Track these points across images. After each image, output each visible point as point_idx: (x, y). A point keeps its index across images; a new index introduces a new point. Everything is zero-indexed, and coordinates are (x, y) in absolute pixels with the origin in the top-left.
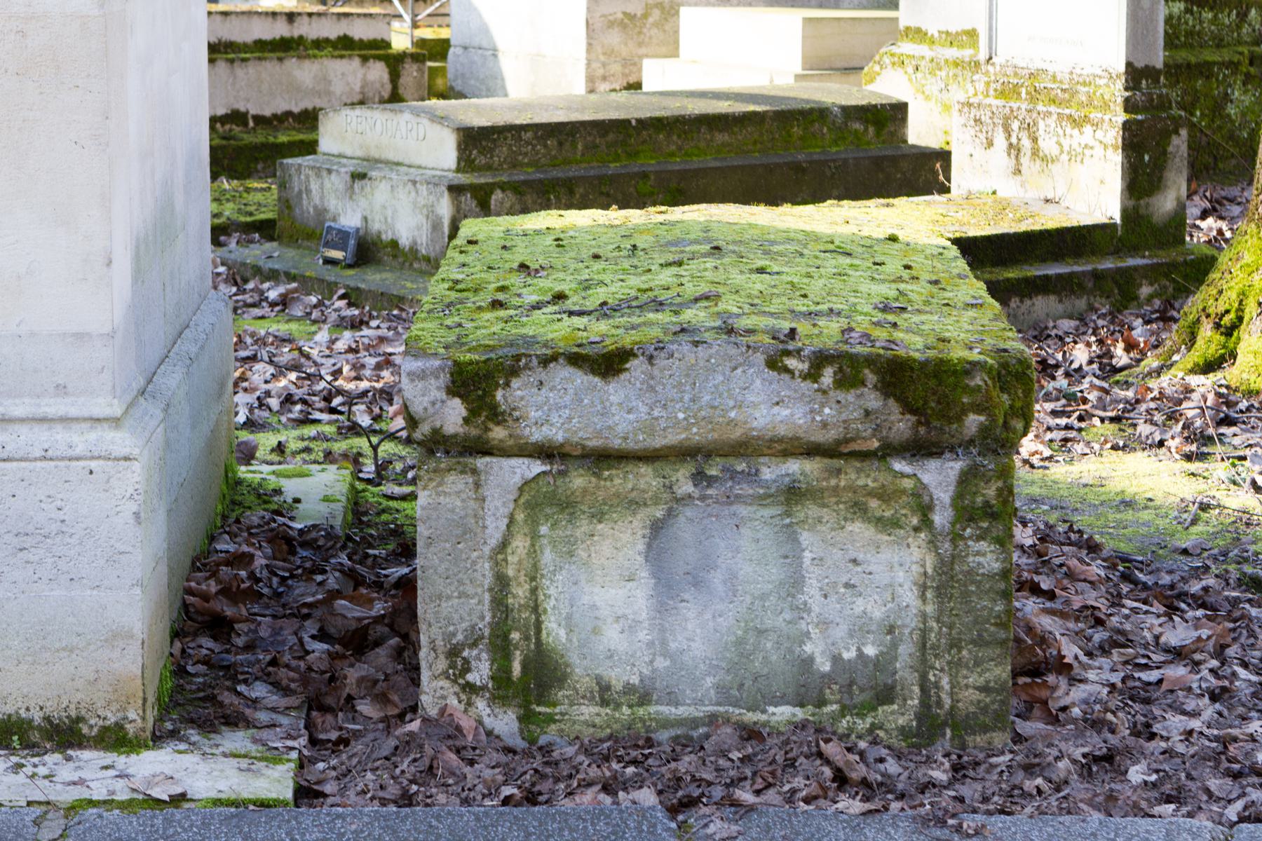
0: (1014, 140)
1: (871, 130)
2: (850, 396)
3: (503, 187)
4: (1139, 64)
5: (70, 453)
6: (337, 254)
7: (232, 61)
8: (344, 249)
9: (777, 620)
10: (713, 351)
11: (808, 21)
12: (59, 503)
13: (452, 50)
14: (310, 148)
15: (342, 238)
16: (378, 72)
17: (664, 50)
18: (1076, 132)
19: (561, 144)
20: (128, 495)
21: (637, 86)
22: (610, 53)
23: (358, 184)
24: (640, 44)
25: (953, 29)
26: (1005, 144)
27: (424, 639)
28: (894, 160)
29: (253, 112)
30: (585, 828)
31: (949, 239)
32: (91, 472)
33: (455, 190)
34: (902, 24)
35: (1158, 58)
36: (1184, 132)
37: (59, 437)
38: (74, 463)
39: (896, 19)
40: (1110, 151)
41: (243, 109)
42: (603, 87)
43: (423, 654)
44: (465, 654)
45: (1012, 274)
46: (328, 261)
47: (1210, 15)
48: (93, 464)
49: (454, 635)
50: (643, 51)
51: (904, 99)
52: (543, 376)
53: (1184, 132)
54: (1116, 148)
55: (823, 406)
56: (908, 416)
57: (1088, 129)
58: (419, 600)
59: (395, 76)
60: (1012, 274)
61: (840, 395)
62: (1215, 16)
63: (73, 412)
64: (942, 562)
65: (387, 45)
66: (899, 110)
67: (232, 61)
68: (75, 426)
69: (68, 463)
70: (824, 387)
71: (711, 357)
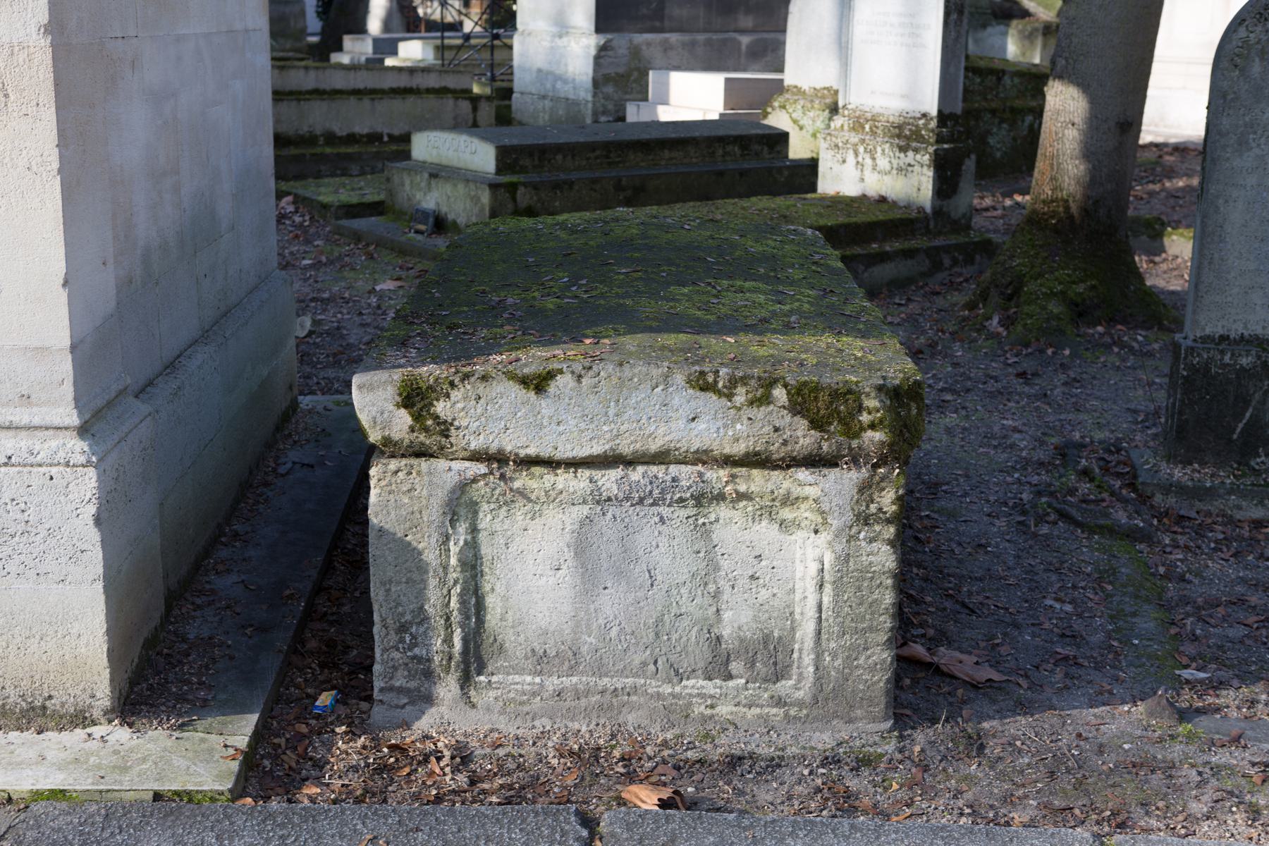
0: (860, 159)
1: (766, 148)
2: (760, 413)
3: (525, 185)
4: (947, 111)
5: (31, 460)
6: (422, 227)
7: (373, 99)
8: (425, 224)
9: (693, 606)
10: (636, 371)
11: (727, 80)
12: (22, 506)
13: (514, 95)
14: (406, 155)
15: (423, 215)
16: (465, 106)
17: (640, 96)
18: (902, 155)
19: (564, 157)
20: (87, 499)
21: (622, 119)
22: (607, 98)
23: (433, 182)
24: (626, 93)
25: (818, 87)
26: (854, 162)
27: (376, 617)
28: (780, 170)
29: (386, 131)
30: (502, 835)
31: (820, 229)
32: (52, 478)
33: (494, 187)
34: (786, 83)
35: (958, 108)
36: (973, 157)
37: (23, 444)
38: (35, 469)
39: (782, 81)
40: (925, 168)
41: (379, 130)
42: (603, 119)
43: (376, 630)
44: (413, 630)
45: (858, 250)
46: (417, 232)
47: (978, 80)
48: (54, 470)
49: (403, 615)
50: (628, 97)
51: (786, 129)
52: (481, 391)
53: (973, 157)
54: (929, 166)
55: (734, 422)
56: (813, 432)
57: (910, 154)
58: (372, 585)
59: (475, 109)
60: (858, 250)
61: (753, 412)
62: (983, 81)
63: (37, 421)
64: (837, 558)
65: (470, 91)
66: (783, 137)
67: (373, 99)
68: (39, 434)
69: (29, 468)
70: (738, 405)
71: (634, 375)
